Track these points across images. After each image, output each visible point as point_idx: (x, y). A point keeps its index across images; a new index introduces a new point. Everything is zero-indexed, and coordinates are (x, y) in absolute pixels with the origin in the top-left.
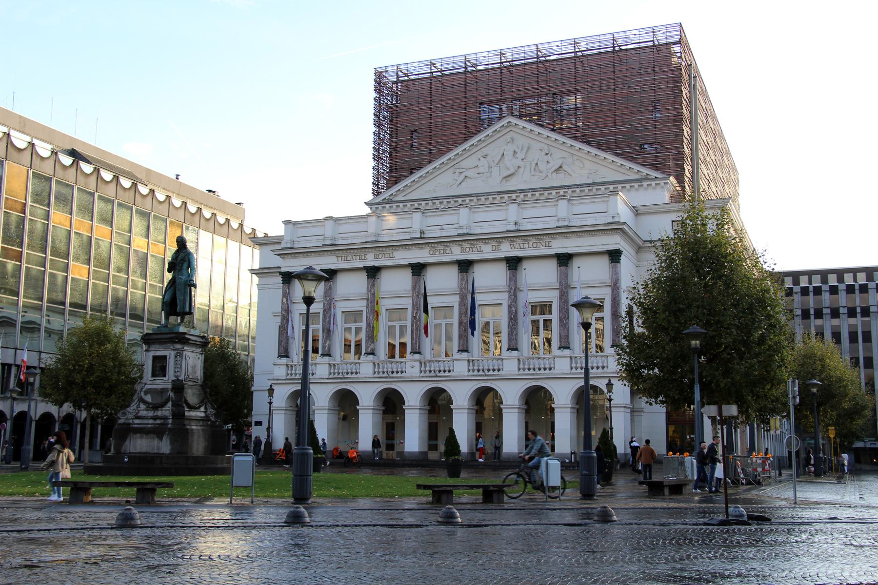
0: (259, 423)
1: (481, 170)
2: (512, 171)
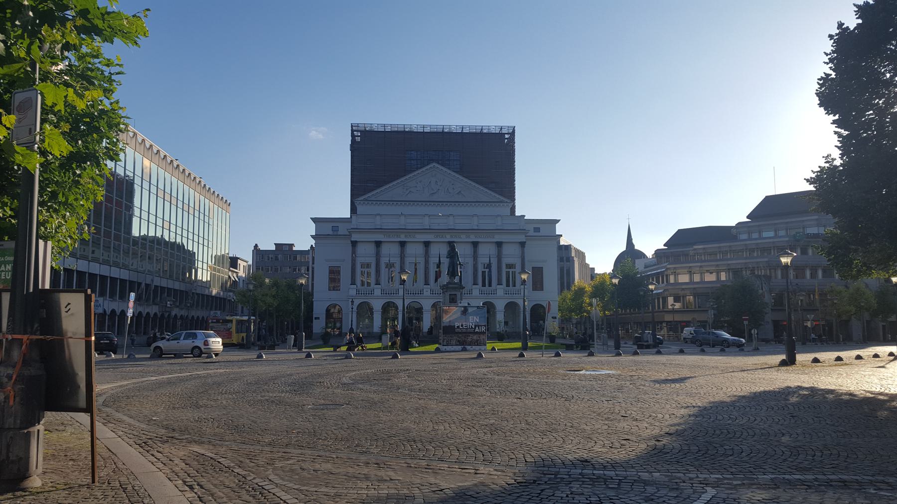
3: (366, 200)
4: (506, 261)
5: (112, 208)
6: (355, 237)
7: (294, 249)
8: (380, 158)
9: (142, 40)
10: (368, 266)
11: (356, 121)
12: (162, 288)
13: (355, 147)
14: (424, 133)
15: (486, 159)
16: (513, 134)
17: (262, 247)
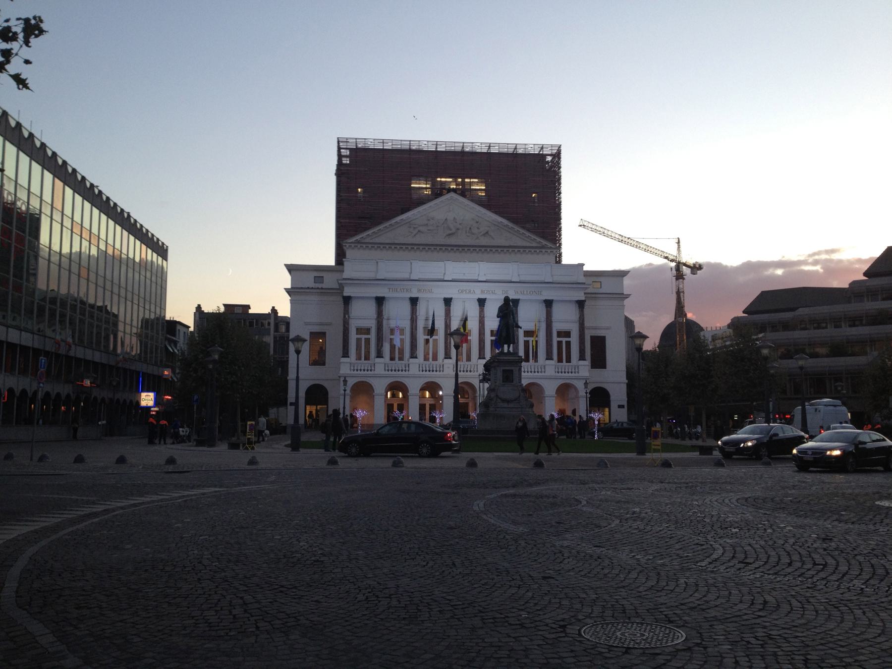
0: (621, 407)
1: (431, 228)
2: (454, 230)
3: (358, 242)
4: (557, 327)
5: (10, 245)
6: (347, 292)
7: (251, 311)
8: (378, 188)
9: (44, 26)
10: (367, 331)
11: (345, 134)
12: (78, 360)
13: (342, 172)
14: (436, 153)
15: (522, 191)
16: (557, 155)
17: (206, 309)
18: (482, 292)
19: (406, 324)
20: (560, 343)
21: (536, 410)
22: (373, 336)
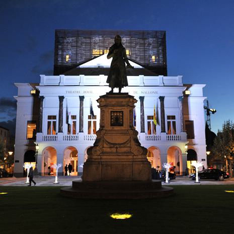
10: (54, 117)
18: (142, 92)
19: (76, 112)
20: (169, 123)
21: (34, 177)
22: (57, 120)
